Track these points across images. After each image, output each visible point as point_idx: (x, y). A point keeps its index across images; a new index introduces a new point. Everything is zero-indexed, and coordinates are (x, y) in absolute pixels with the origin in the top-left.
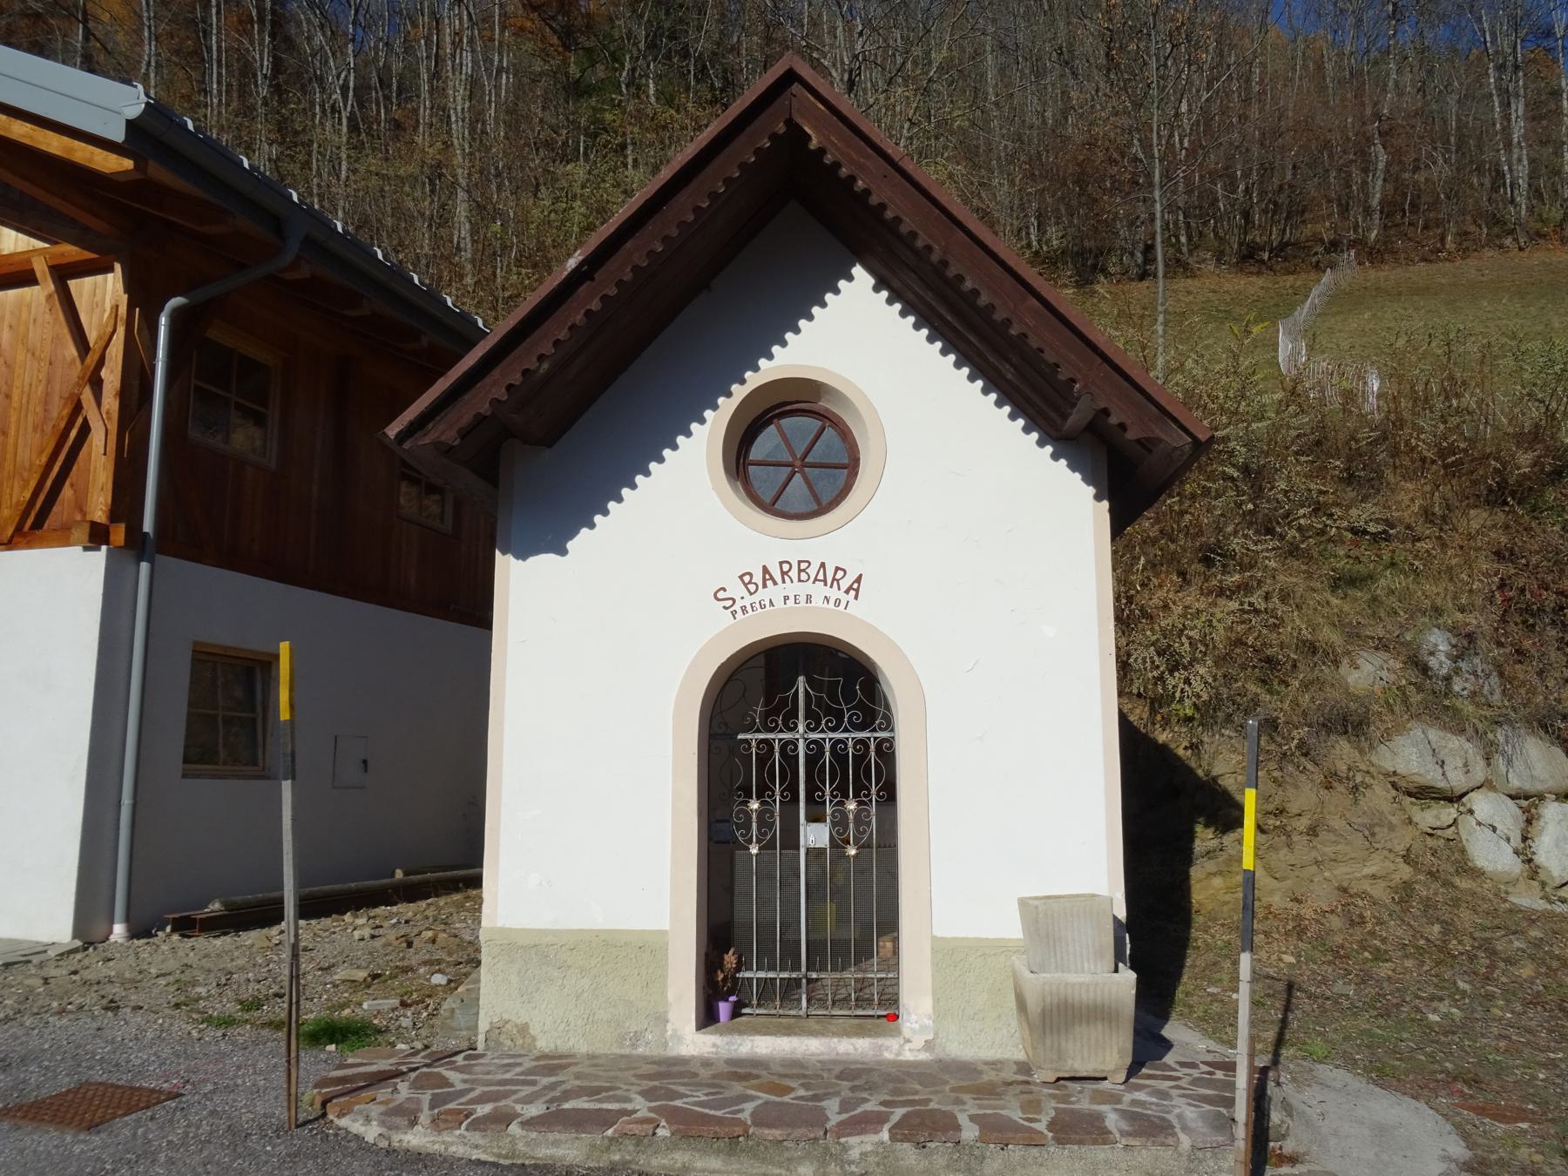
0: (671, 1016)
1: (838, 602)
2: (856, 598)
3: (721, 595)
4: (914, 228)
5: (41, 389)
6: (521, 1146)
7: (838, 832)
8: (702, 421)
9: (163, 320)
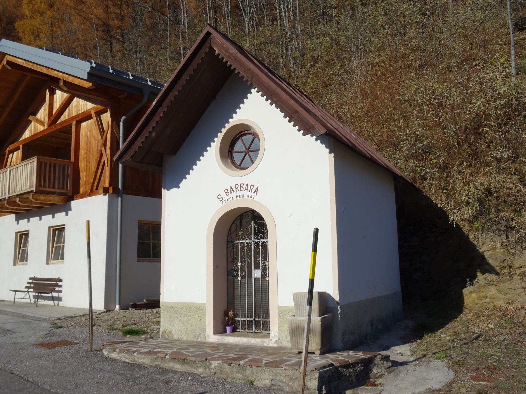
0: (207, 329)
1: (251, 196)
2: (257, 194)
3: (219, 197)
4: (243, 74)
5: (96, 149)
6: (136, 359)
7: (263, 272)
8: (214, 142)
9: (121, 124)
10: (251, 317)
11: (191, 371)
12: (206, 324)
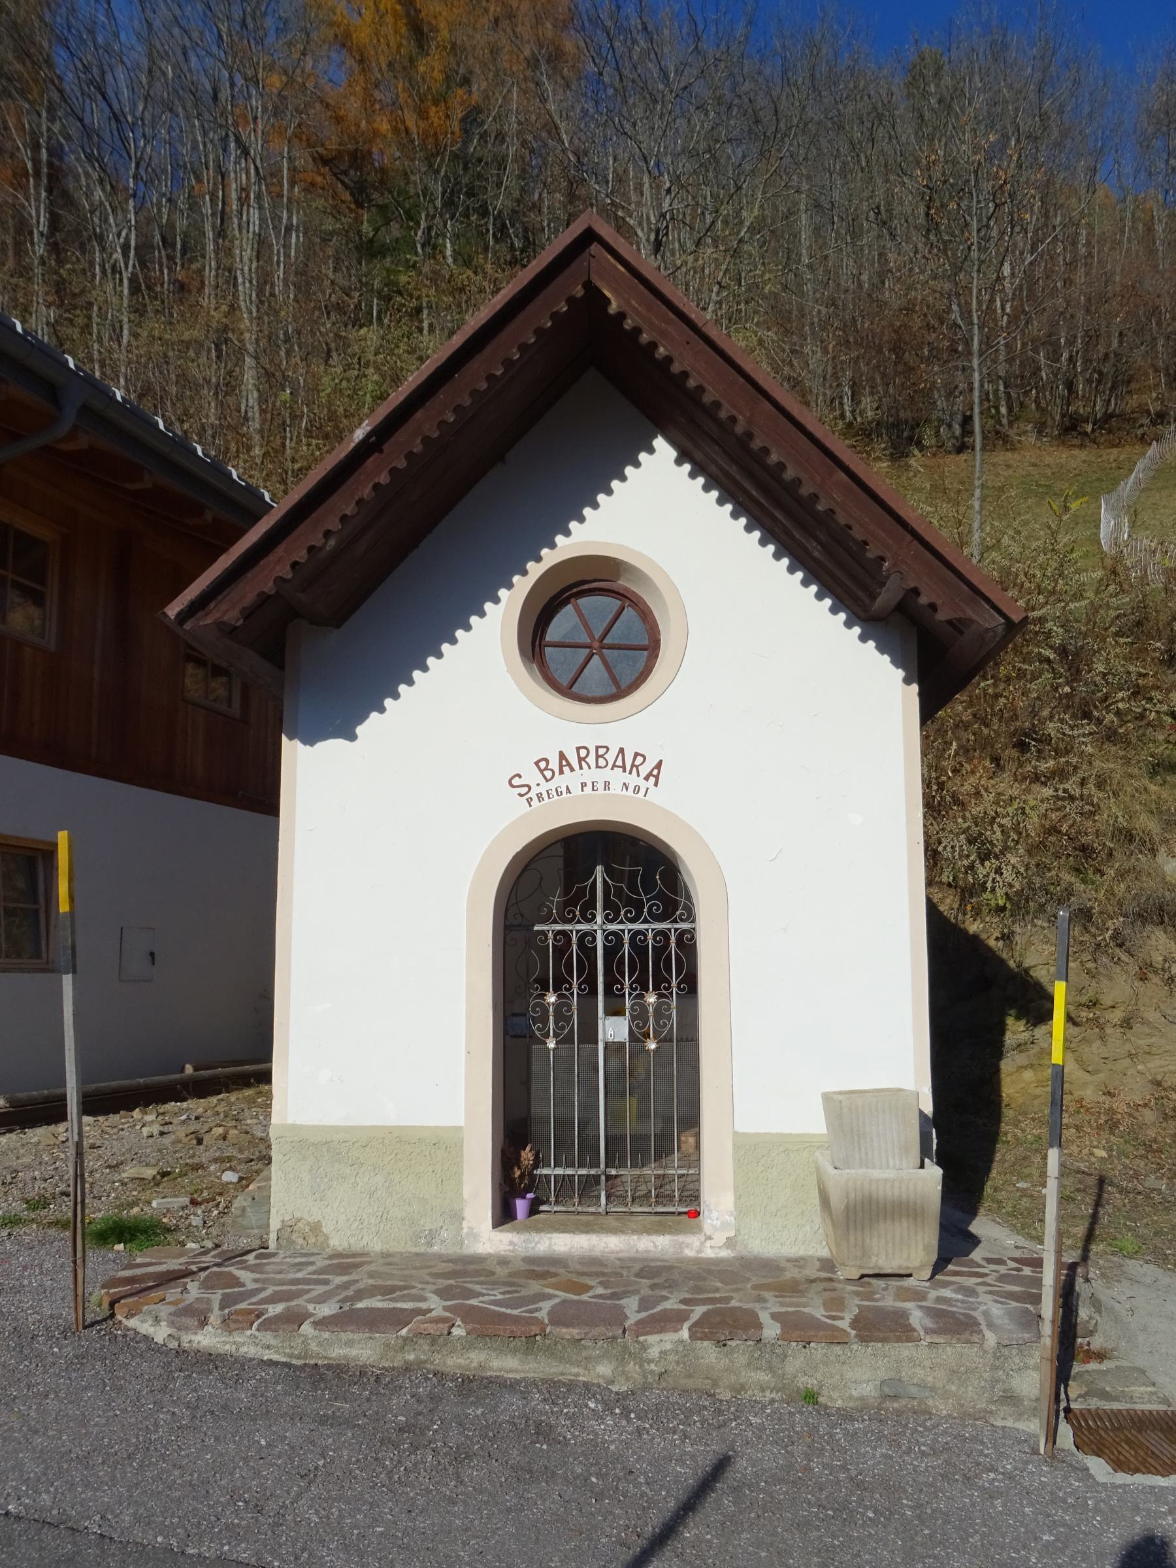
0: (467, 1213)
2: (656, 784)
3: (516, 782)
6: (313, 1346)
10: (595, 1163)
11: (562, 1374)
12: (466, 1196)
